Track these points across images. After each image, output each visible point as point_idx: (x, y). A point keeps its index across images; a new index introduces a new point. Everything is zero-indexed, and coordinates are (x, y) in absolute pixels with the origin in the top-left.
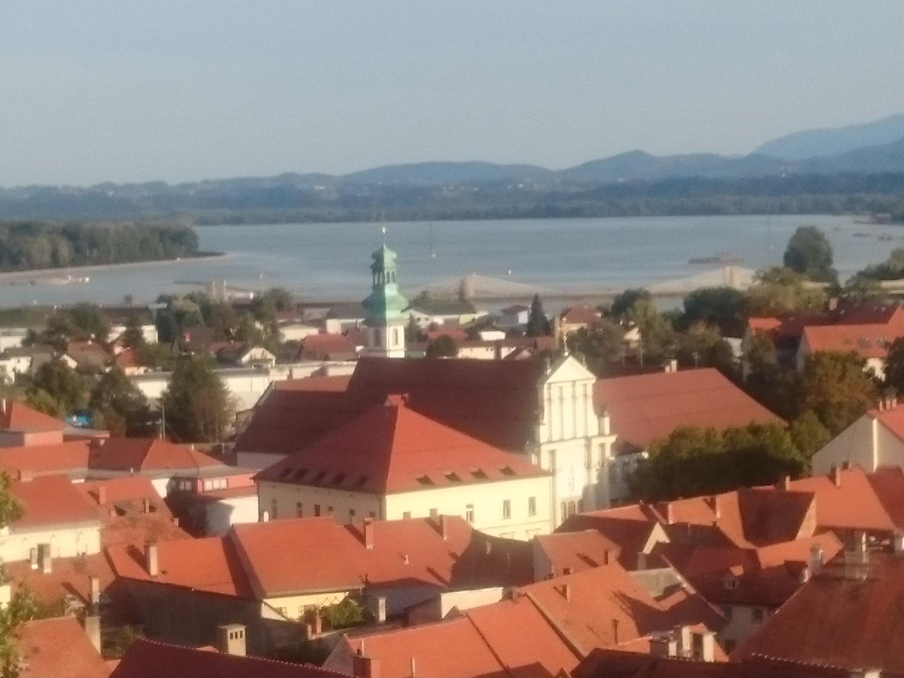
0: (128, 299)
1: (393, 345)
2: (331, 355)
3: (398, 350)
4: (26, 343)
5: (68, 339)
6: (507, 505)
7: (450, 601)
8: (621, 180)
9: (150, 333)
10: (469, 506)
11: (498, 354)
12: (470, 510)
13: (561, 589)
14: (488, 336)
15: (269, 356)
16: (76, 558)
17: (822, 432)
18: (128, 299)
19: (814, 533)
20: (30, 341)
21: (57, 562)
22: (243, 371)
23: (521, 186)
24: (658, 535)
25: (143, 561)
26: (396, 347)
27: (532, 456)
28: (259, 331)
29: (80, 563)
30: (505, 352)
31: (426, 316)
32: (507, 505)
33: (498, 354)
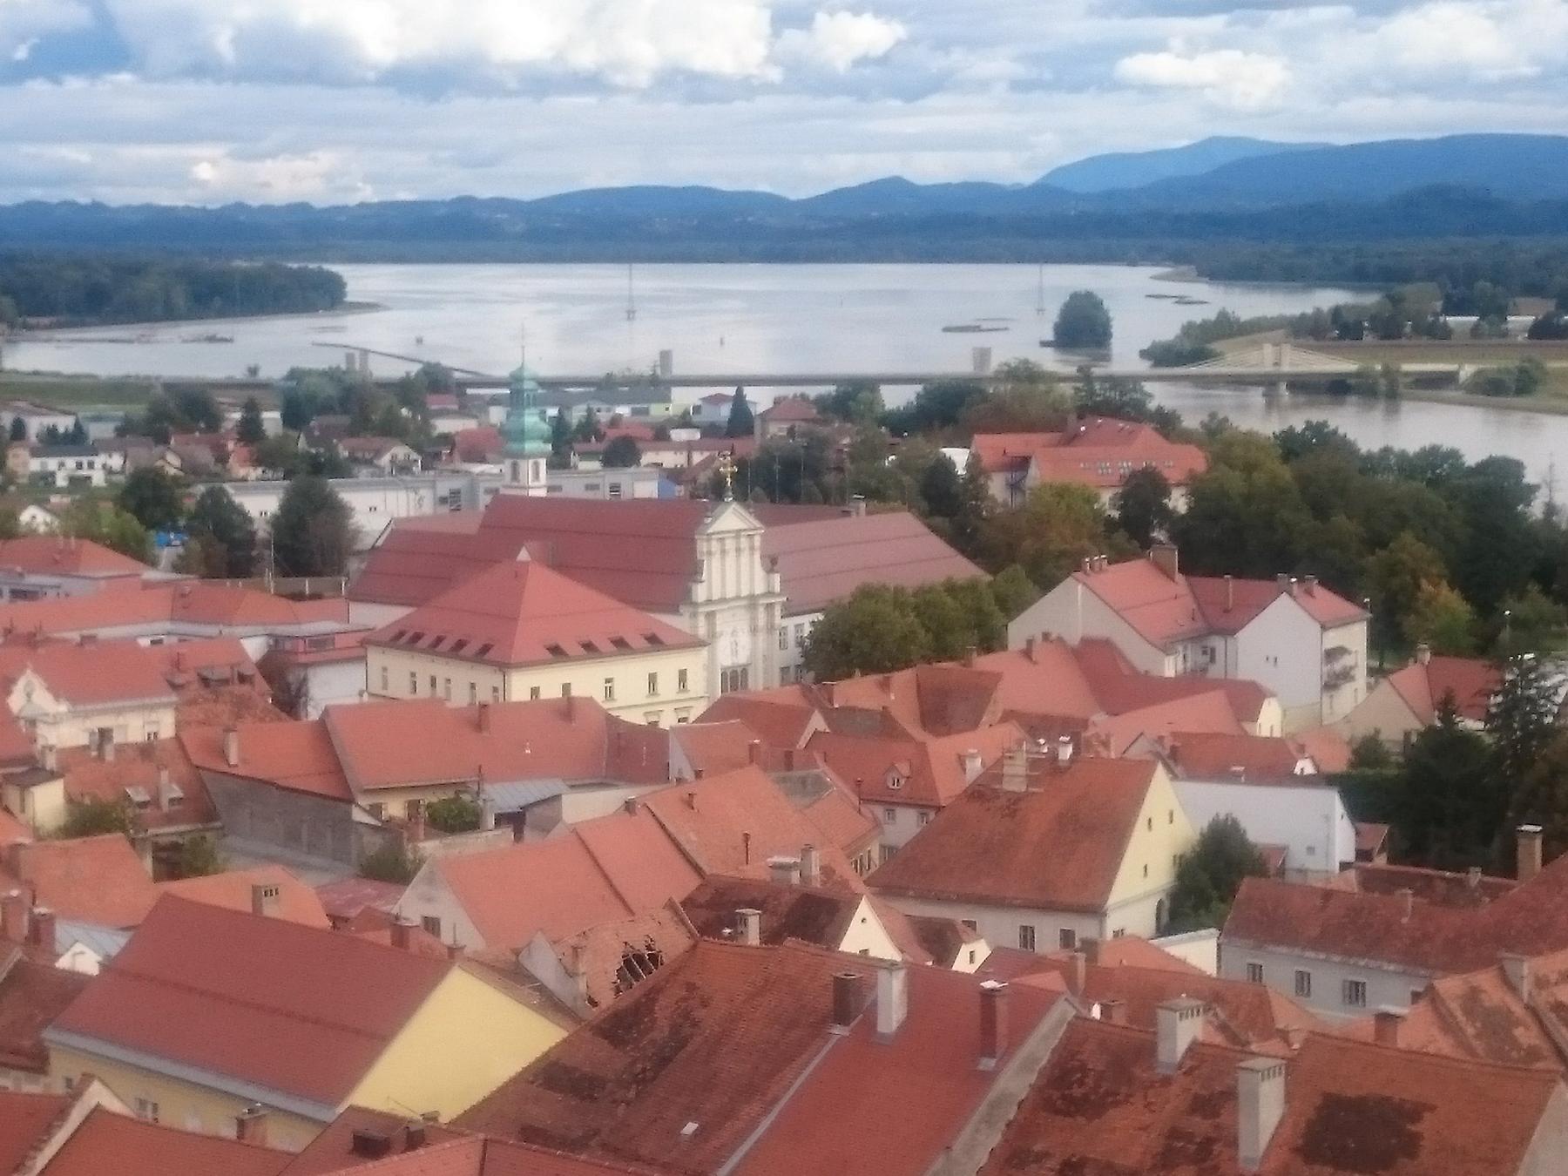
0: (253, 371)
1: (533, 481)
2: (489, 456)
3: (539, 487)
4: (121, 432)
5: (171, 428)
6: (652, 679)
7: (976, 751)
8: (875, 214)
9: (271, 419)
10: (608, 681)
11: (689, 458)
12: (609, 685)
13: (1104, 737)
14: (679, 435)
15: (414, 456)
16: (142, 743)
17: (1030, 587)
18: (253, 371)
19: (1001, 718)
20: (126, 430)
21: (121, 749)
22: (381, 481)
23: (750, 219)
24: (817, 722)
25: (222, 754)
26: (536, 484)
27: (1372, 289)
28: (407, 419)
29: (147, 750)
30: (697, 458)
31: (607, 406)
32: (652, 679)
33: (689, 458)
